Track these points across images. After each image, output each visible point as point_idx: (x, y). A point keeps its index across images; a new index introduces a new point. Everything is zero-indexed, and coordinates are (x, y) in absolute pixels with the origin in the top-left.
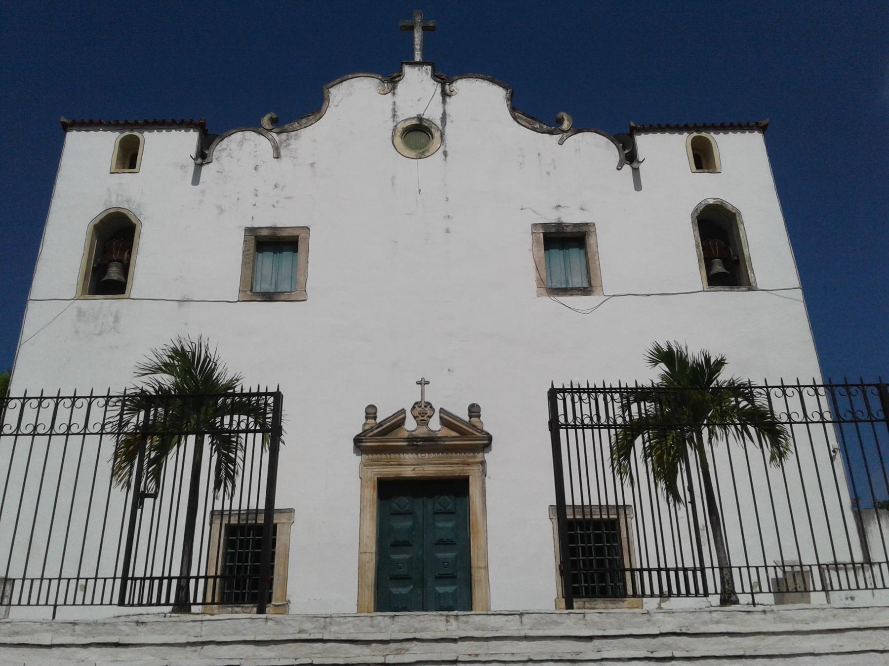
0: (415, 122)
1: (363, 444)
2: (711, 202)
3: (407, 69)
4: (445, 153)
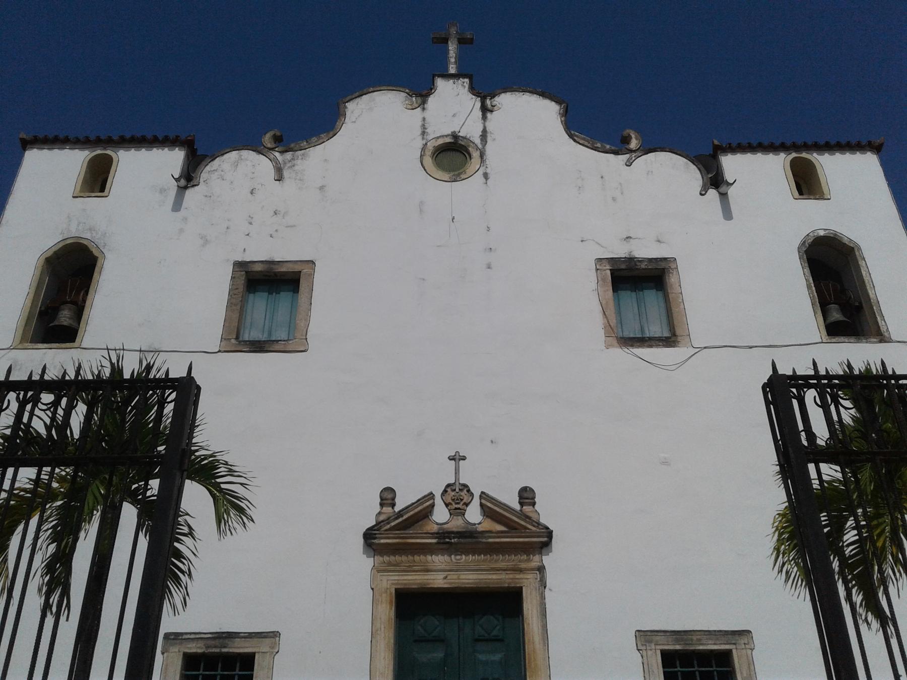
0: (448, 140)
1: (376, 541)
2: (822, 233)
3: (440, 83)
4: (486, 176)
